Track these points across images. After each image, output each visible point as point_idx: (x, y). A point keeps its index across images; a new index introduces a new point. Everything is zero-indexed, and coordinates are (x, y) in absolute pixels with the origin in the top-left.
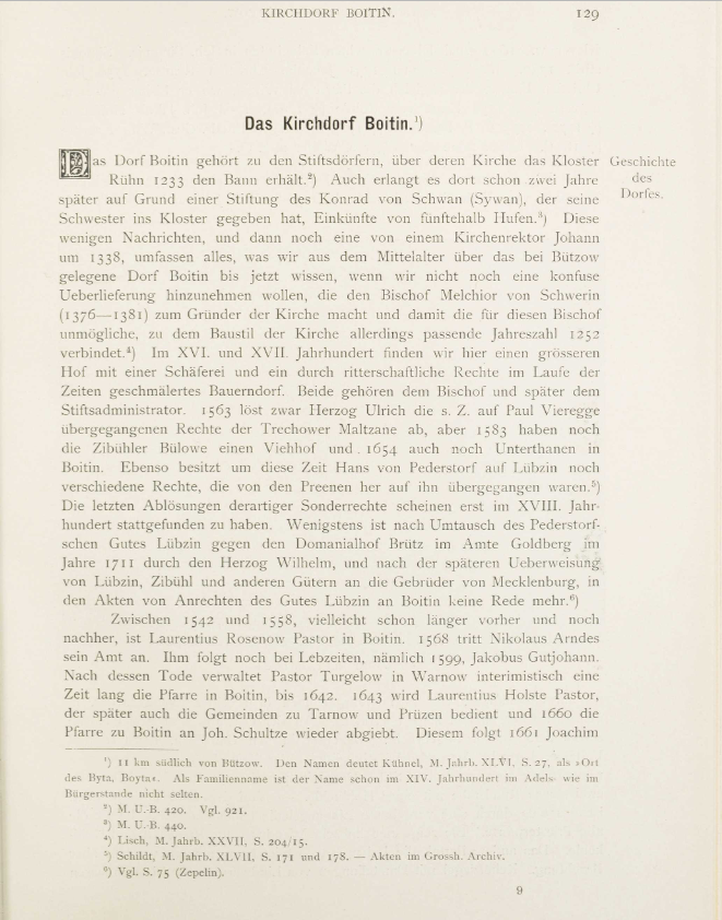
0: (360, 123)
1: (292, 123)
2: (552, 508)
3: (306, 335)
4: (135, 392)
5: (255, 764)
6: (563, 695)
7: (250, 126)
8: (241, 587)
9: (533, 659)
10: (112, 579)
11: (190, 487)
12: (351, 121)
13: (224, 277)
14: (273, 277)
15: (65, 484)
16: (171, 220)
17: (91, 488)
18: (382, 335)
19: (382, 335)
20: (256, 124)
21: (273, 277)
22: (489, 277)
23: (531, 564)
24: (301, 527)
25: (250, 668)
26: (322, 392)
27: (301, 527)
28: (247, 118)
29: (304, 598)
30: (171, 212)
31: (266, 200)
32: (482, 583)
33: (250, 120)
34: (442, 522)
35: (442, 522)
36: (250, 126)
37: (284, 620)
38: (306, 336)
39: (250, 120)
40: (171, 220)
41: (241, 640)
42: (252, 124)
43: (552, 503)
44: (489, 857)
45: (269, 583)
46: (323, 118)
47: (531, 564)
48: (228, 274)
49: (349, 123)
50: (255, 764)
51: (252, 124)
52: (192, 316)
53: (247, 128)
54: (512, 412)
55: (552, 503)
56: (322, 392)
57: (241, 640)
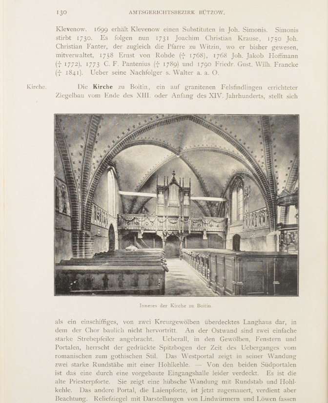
2: (147, 96)
3: (31, 87)
5: (82, 30)
6: (126, 64)
13: (252, 48)
14: (212, 391)
15: (141, 54)
18: (267, 391)
19: (267, 391)
21: (212, 391)
23: (251, 348)
24: (188, 357)
25: (253, 361)
26: (248, 365)
27: (188, 357)
29: (86, 380)
31: (212, 382)
37: (109, 55)
38: (31, 88)
43: (147, 94)
44: (135, 12)
47: (251, 348)
48: (253, 46)
50: (82, 30)
54: (125, 65)
55: (147, 94)
56: (248, 365)
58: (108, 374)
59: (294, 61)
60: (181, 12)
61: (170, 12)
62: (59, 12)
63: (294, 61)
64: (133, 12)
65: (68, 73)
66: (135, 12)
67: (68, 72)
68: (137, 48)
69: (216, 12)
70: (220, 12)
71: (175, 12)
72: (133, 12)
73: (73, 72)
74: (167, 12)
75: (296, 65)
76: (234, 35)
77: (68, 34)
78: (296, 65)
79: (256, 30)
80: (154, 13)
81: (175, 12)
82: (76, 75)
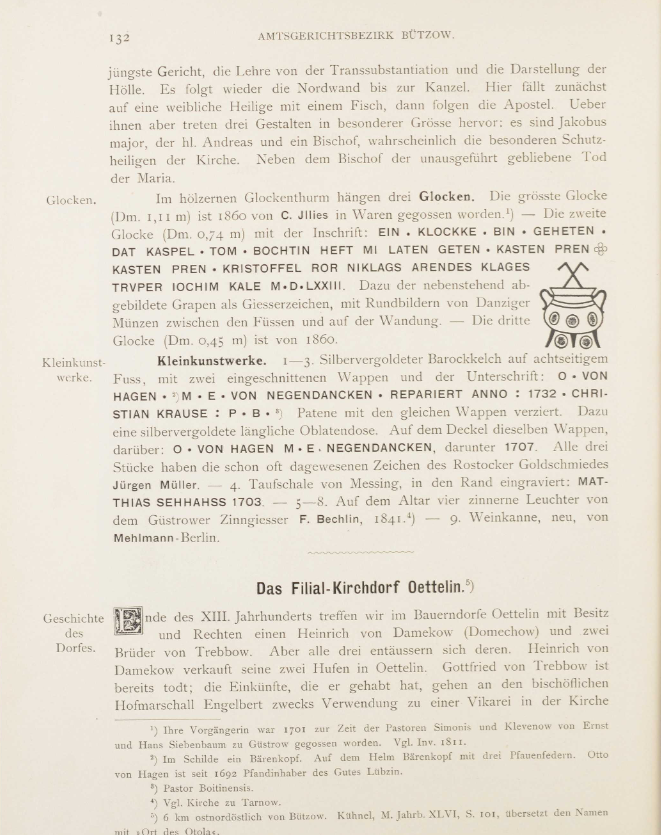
0: (403, 587)
1: (341, 588)
4: (544, 360)
5: (274, 803)
7: (261, 591)
8: (351, 75)
9: (424, 198)
10: (378, 68)
11: (297, 125)
12: (396, 585)
16: (51, 365)
17: (510, 378)
20: (266, 589)
22: (460, 360)
28: (259, 583)
30: (51, 357)
32: (465, 304)
33: (261, 586)
34: (478, 374)
35: (478, 374)
36: (261, 591)
39: (261, 586)
40: (51, 365)
41: (467, 466)
42: (262, 588)
44: (271, 36)
45: (542, 141)
46: (369, 583)
49: (393, 587)
50: (274, 803)
51: (262, 588)
52: (176, 306)
53: (259, 593)
57: (467, 466)
58: (592, 702)
59: (602, 693)
60: (366, 36)
61: (343, 36)
62: (115, 39)
63: (602, 693)
64: (265, 36)
65: (379, 520)
66: (271, 36)
67: (380, 518)
68: (407, 415)
69: (436, 35)
70: (446, 34)
71: (353, 36)
72: (265, 36)
73: (389, 518)
74: (337, 36)
75: (605, 702)
76: (187, 629)
77: (446, 259)
78: (605, 702)
79: (248, 468)
80: (310, 37)
81: (353, 36)
82: (396, 524)
